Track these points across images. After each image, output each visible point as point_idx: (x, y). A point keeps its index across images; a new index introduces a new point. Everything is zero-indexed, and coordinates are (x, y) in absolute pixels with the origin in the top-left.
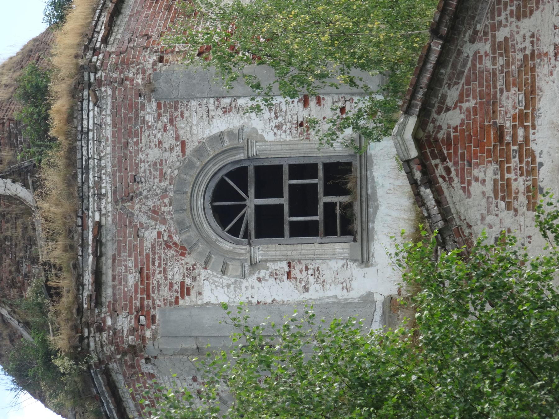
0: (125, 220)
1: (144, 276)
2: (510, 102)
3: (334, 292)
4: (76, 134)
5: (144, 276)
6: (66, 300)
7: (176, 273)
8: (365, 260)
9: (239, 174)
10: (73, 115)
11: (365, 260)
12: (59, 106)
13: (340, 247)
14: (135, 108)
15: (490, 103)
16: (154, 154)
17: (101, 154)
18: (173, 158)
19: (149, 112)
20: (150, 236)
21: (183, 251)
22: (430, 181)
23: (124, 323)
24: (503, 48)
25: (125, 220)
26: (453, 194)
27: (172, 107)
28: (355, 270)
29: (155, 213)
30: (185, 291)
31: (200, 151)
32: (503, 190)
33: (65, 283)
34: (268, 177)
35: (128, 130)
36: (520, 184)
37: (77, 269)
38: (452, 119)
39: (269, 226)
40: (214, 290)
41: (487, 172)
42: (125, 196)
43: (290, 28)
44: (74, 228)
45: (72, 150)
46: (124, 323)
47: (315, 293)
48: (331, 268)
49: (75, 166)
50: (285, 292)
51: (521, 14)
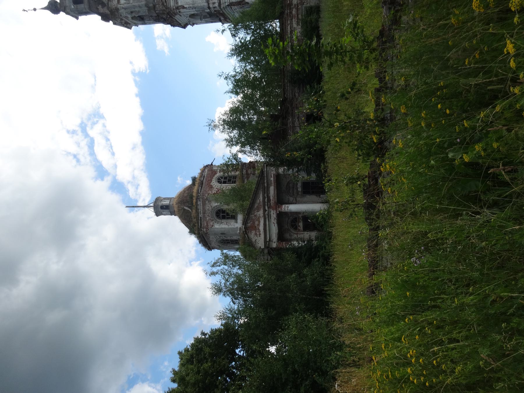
0: (204, 216)
1: (207, 224)
2: (257, 223)
3: (233, 226)
4: (197, 205)
5: (207, 224)
6: (197, 227)
7: (211, 224)
8: (237, 222)
9: (219, 210)
10: (196, 202)
11: (237, 222)
12: (194, 201)
13: (234, 221)
14: (205, 202)
15: (254, 223)
16: (208, 208)
17: (200, 207)
18: (210, 208)
19: (207, 202)
20: (208, 219)
21: (212, 221)
22: (246, 234)
23: (205, 230)
24: (256, 216)
25: (204, 216)
26: (249, 234)
27: (210, 202)
28: (235, 224)
29: (208, 216)
30: (213, 226)
31: (214, 208)
32: (256, 234)
33: (196, 225)
34: (224, 211)
35: (204, 204)
36: (258, 233)
37: (198, 223)
38: (249, 225)
39: (224, 218)
40: (217, 226)
41: (254, 232)
42: (204, 213)
43: (238, 373)
44: (197, 217)
45: (197, 207)
46: (205, 230)
47: (230, 227)
48: (232, 223)
49: (197, 209)
50: (226, 226)
51: (258, 211)
